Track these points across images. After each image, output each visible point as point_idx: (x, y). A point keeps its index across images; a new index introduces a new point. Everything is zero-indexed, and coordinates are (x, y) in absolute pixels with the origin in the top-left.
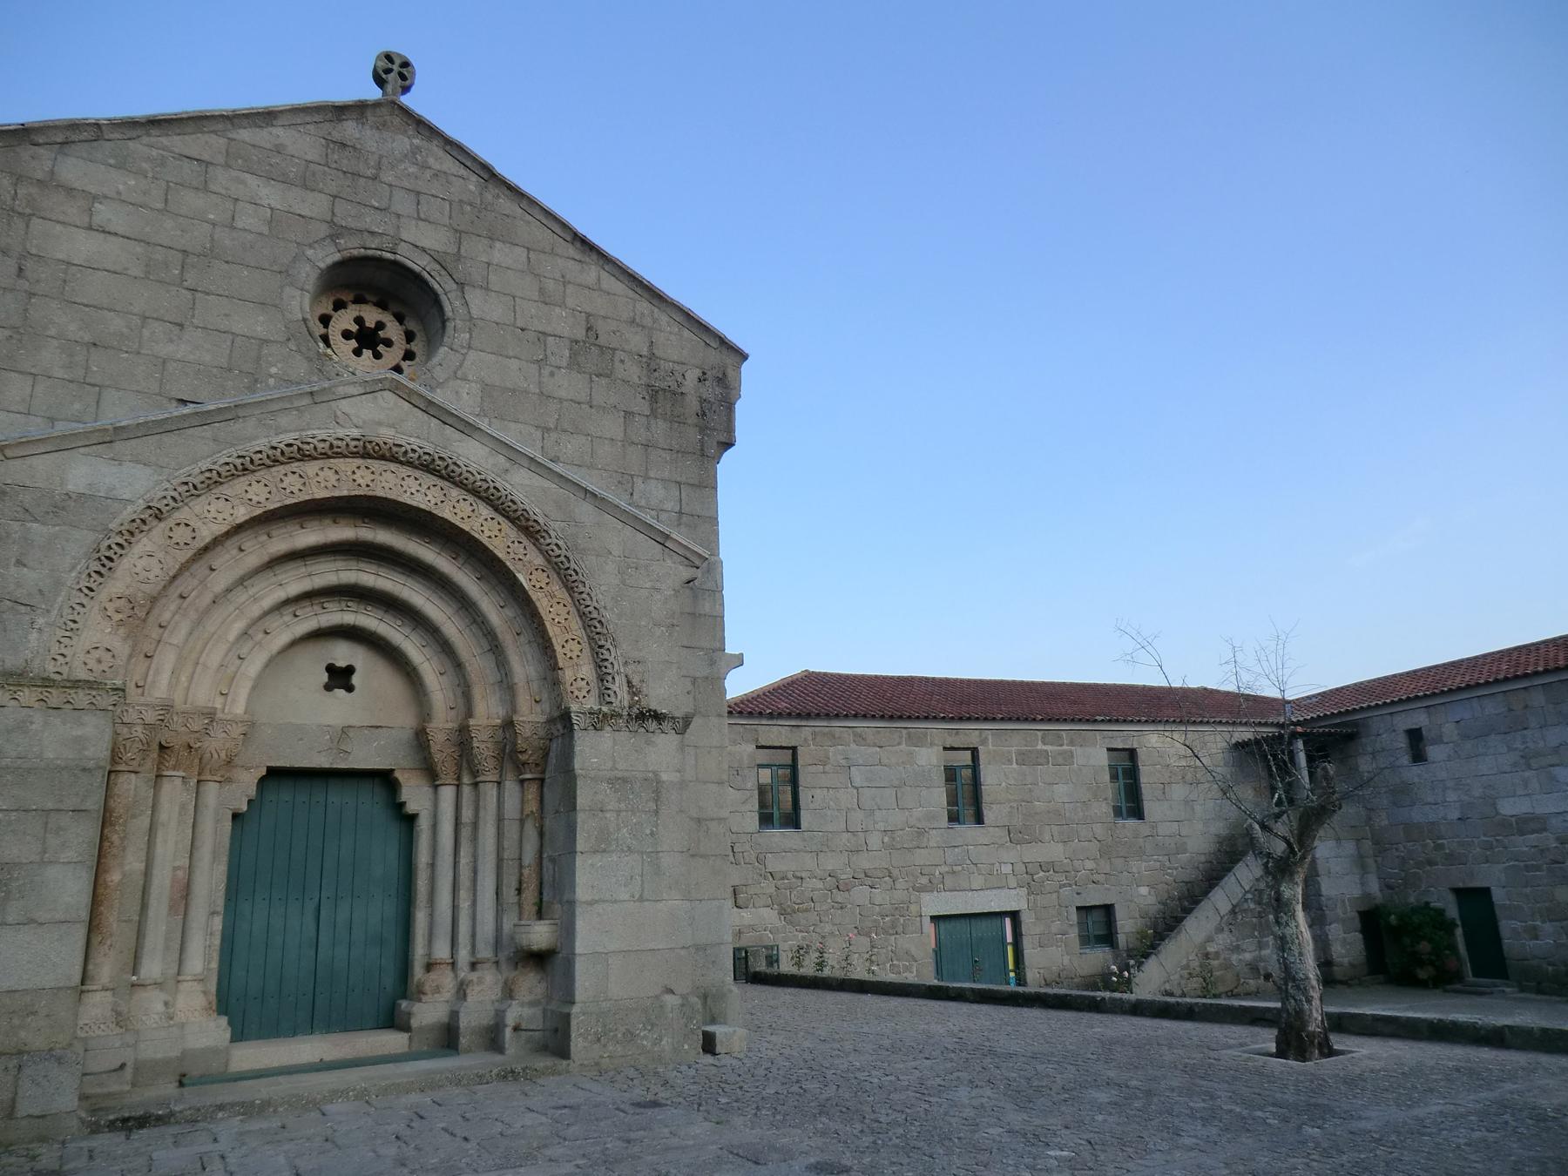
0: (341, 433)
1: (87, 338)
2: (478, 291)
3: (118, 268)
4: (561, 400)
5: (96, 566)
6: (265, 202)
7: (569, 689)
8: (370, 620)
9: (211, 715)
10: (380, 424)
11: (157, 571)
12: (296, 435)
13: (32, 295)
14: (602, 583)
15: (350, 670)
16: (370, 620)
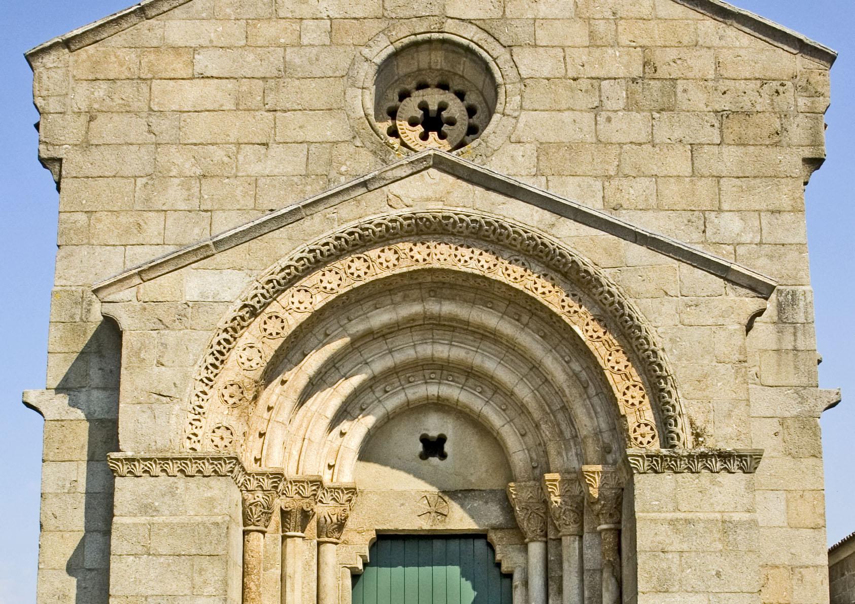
0: (393, 214)
1: (199, 172)
2: (527, 50)
3: (216, 106)
4: (621, 145)
5: (211, 360)
6: (324, 15)
7: (632, 435)
8: (451, 392)
9: (318, 483)
10: (428, 200)
11: (256, 359)
12: (355, 223)
13: (158, 144)
14: (658, 323)
15: (442, 439)
16: (451, 392)
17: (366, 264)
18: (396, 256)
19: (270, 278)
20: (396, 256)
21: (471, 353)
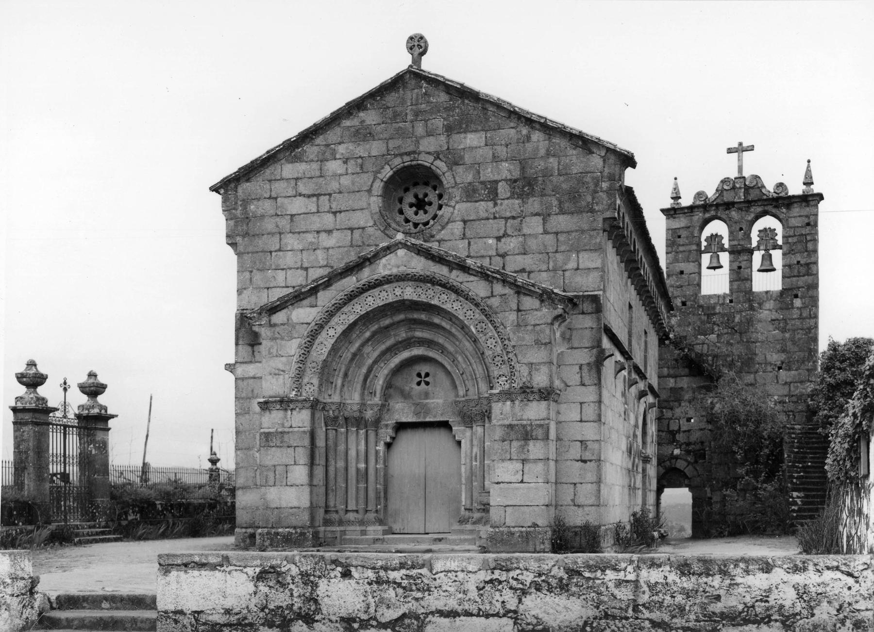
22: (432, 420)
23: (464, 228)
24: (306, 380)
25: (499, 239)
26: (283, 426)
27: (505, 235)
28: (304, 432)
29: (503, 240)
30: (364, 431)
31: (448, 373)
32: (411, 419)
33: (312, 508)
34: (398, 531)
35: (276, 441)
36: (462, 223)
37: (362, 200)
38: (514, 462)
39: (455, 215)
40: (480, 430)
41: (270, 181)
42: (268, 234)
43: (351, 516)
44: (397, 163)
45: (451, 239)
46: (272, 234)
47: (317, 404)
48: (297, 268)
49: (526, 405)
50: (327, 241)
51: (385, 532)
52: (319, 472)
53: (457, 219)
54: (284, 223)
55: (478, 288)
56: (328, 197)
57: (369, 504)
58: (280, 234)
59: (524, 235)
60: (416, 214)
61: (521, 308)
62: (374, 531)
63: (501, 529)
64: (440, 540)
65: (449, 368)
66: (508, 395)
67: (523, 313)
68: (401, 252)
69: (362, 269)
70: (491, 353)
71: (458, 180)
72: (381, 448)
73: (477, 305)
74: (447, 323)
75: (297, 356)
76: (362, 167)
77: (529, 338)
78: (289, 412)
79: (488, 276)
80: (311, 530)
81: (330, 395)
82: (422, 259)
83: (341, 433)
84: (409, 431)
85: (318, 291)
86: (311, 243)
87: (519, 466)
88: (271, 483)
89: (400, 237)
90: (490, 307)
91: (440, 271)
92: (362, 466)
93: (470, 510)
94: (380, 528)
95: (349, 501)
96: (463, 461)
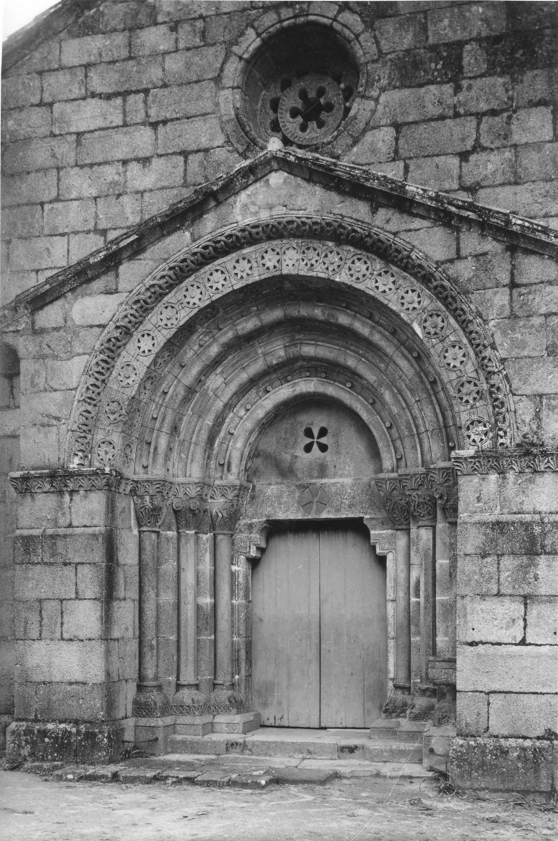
17: (223, 276)
18: (250, 265)
19: (136, 298)
20: (250, 265)
21: (335, 351)
22: (331, 516)
23: (397, 139)
24: (99, 436)
25: (464, 156)
26: (56, 524)
27: (478, 147)
28: (94, 536)
29: (473, 158)
30: (210, 535)
31: (363, 428)
32: (294, 514)
33: (110, 688)
34: (271, 722)
35: (42, 553)
36: (391, 131)
37: (203, 98)
38: (507, 600)
39: (378, 115)
40: (425, 534)
41: (40, 73)
42: (38, 171)
43: (186, 696)
44: (268, 23)
45: (371, 153)
46: (44, 170)
47: (119, 483)
48: (88, 232)
49: (531, 481)
50: (140, 178)
51: (249, 728)
52: (125, 613)
53: (383, 122)
54: (65, 150)
55: (429, 243)
56: (142, 95)
57: (220, 673)
58: (59, 169)
59: (515, 146)
60: (303, 128)
61: (518, 280)
62: (228, 726)
63: (480, 740)
64: (352, 750)
65: (365, 416)
66: (492, 460)
67: (523, 290)
68: (277, 178)
69: (201, 216)
70: (453, 376)
71: (385, 46)
72: (241, 568)
73: (426, 279)
74: (364, 324)
75: (82, 389)
76: (203, 34)
77: (535, 344)
78: (67, 498)
79: (450, 215)
80: (105, 728)
81: (146, 467)
82: (318, 189)
83: (168, 539)
84: (290, 537)
85: (120, 263)
86: (114, 184)
87: (517, 608)
88: (35, 634)
89: (274, 145)
90: (454, 281)
91: (353, 212)
92: (207, 601)
93: (405, 689)
94: (238, 719)
95: (182, 668)
96: (390, 595)
